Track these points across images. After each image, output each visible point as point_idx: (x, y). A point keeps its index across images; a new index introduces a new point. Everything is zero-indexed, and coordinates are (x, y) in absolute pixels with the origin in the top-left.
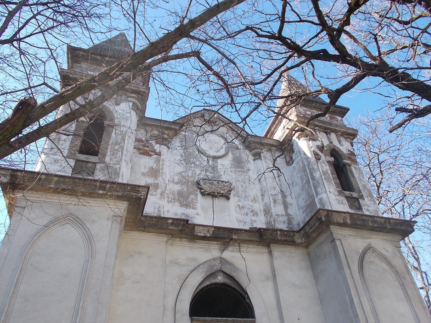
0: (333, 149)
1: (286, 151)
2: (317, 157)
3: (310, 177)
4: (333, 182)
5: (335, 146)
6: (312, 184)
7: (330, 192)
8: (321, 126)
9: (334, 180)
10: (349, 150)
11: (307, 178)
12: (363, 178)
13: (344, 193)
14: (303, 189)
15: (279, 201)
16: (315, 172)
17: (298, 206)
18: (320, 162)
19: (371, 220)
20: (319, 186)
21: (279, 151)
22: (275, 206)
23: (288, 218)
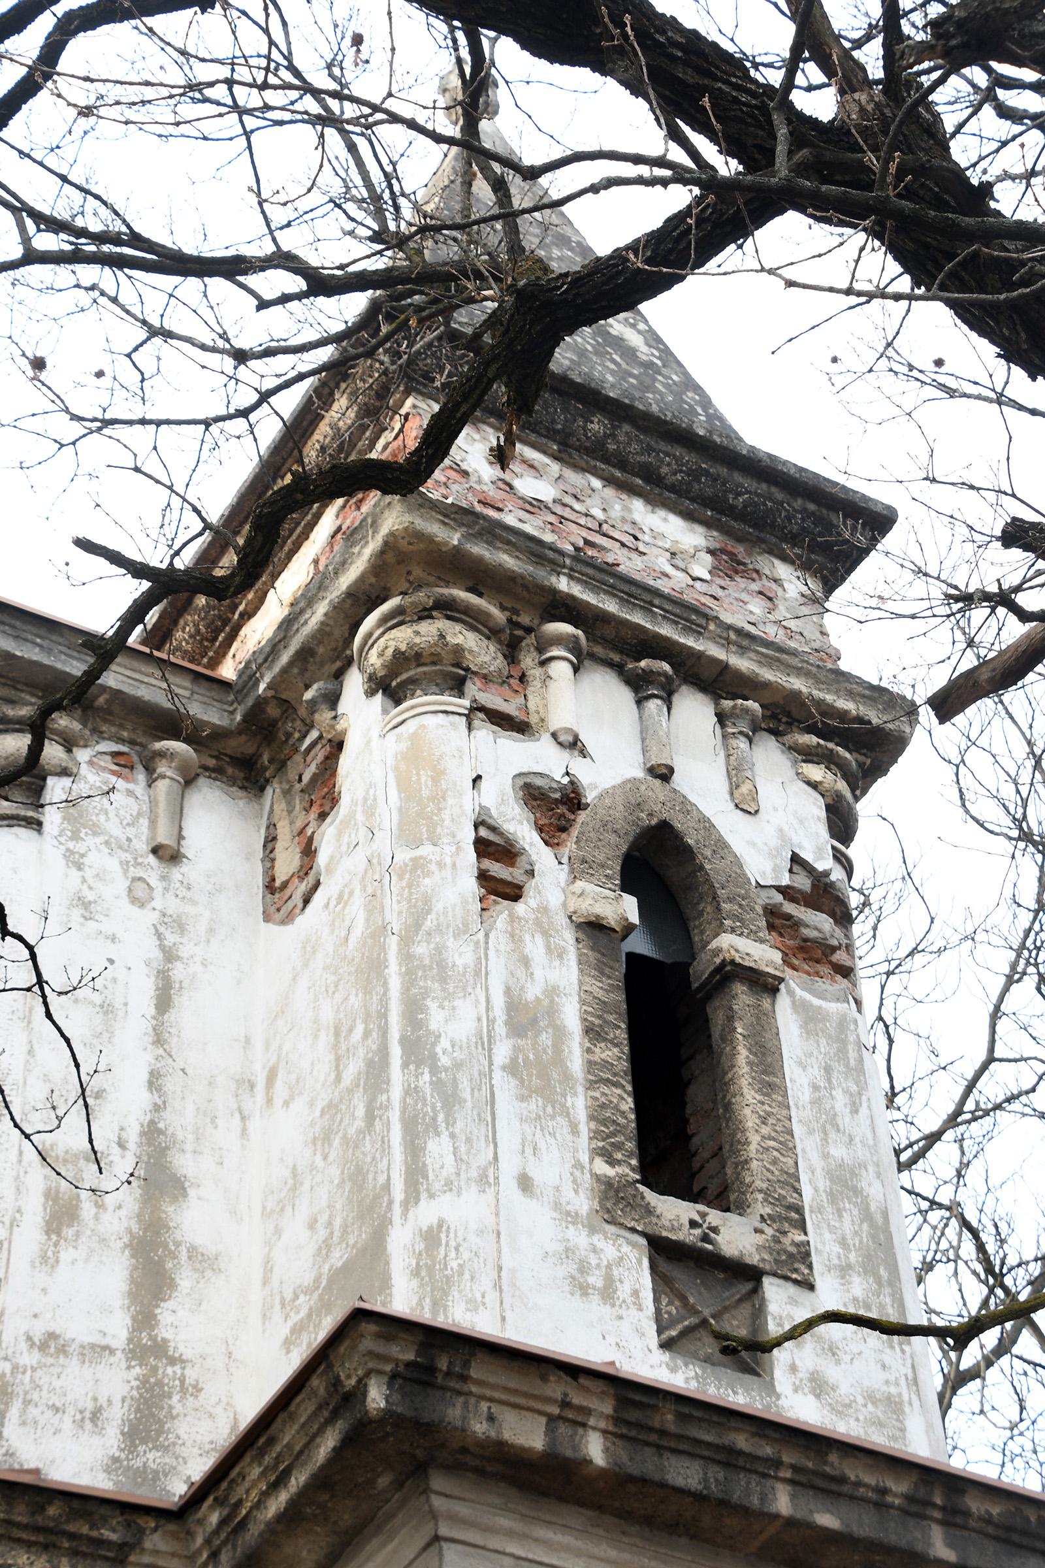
0: (665, 827)
1: (286, 793)
2: (497, 869)
3: (395, 1034)
4: (579, 1104)
5: (686, 806)
6: (396, 1092)
7: (525, 1183)
8: (604, 618)
9: (591, 1085)
10: (795, 859)
11: (373, 1043)
12: (855, 1111)
13: (649, 1211)
14: (327, 1137)
15: (107, 1217)
16: (450, 996)
17: (265, 1282)
18: (512, 917)
19: (795, 1468)
20: (450, 1122)
21: (232, 781)
22: (47, 1261)
23: (144, 1381)
